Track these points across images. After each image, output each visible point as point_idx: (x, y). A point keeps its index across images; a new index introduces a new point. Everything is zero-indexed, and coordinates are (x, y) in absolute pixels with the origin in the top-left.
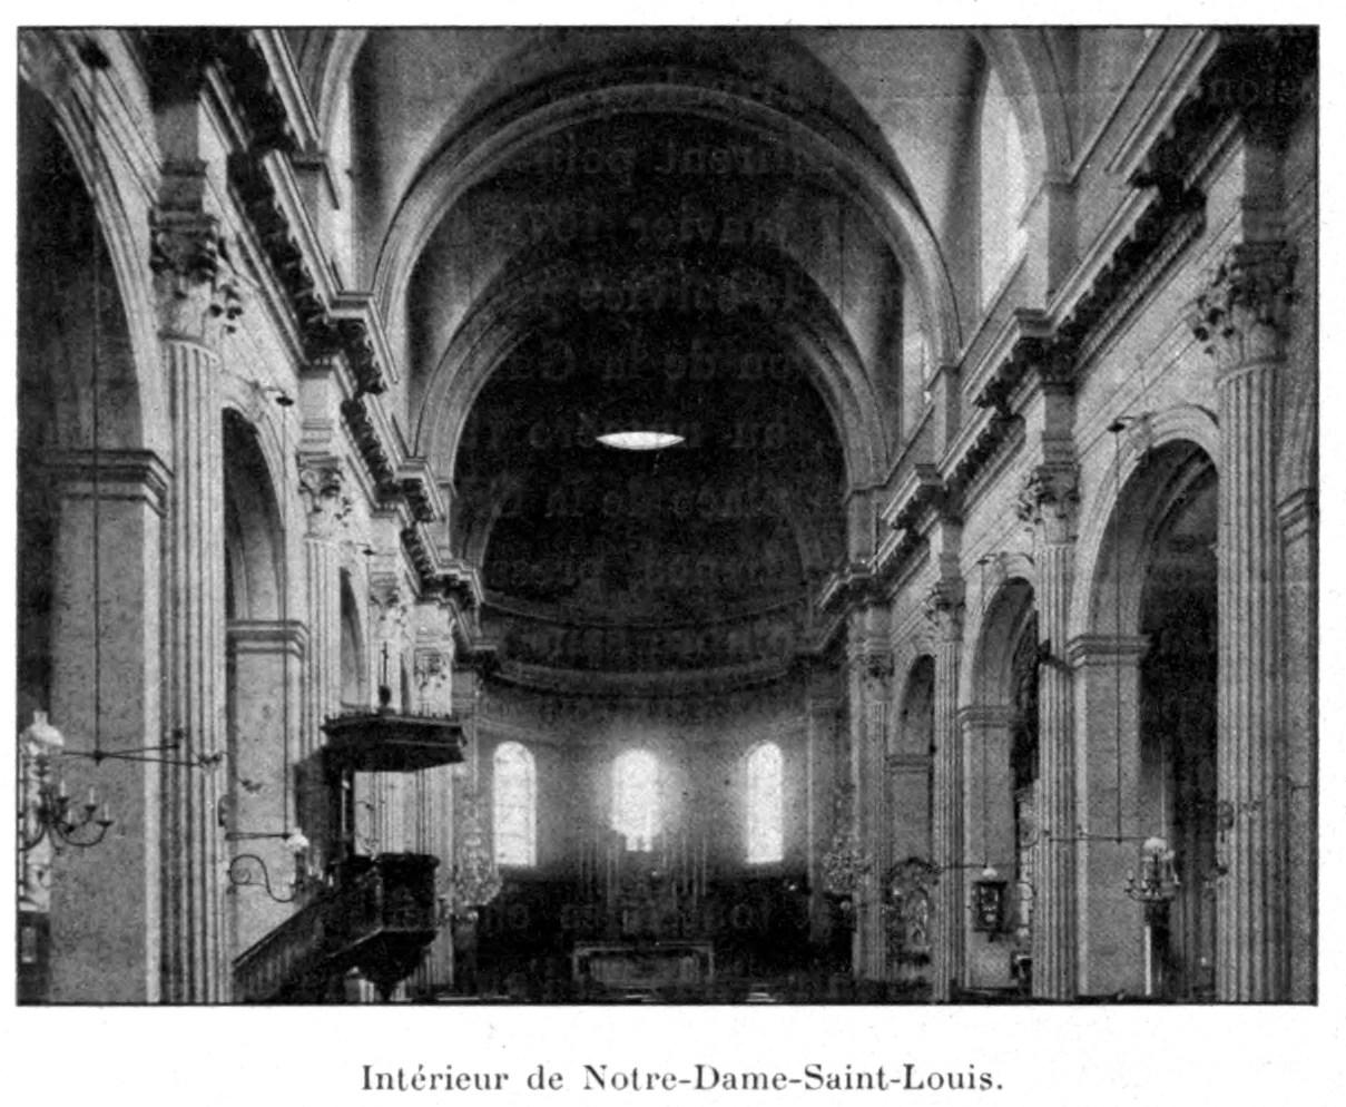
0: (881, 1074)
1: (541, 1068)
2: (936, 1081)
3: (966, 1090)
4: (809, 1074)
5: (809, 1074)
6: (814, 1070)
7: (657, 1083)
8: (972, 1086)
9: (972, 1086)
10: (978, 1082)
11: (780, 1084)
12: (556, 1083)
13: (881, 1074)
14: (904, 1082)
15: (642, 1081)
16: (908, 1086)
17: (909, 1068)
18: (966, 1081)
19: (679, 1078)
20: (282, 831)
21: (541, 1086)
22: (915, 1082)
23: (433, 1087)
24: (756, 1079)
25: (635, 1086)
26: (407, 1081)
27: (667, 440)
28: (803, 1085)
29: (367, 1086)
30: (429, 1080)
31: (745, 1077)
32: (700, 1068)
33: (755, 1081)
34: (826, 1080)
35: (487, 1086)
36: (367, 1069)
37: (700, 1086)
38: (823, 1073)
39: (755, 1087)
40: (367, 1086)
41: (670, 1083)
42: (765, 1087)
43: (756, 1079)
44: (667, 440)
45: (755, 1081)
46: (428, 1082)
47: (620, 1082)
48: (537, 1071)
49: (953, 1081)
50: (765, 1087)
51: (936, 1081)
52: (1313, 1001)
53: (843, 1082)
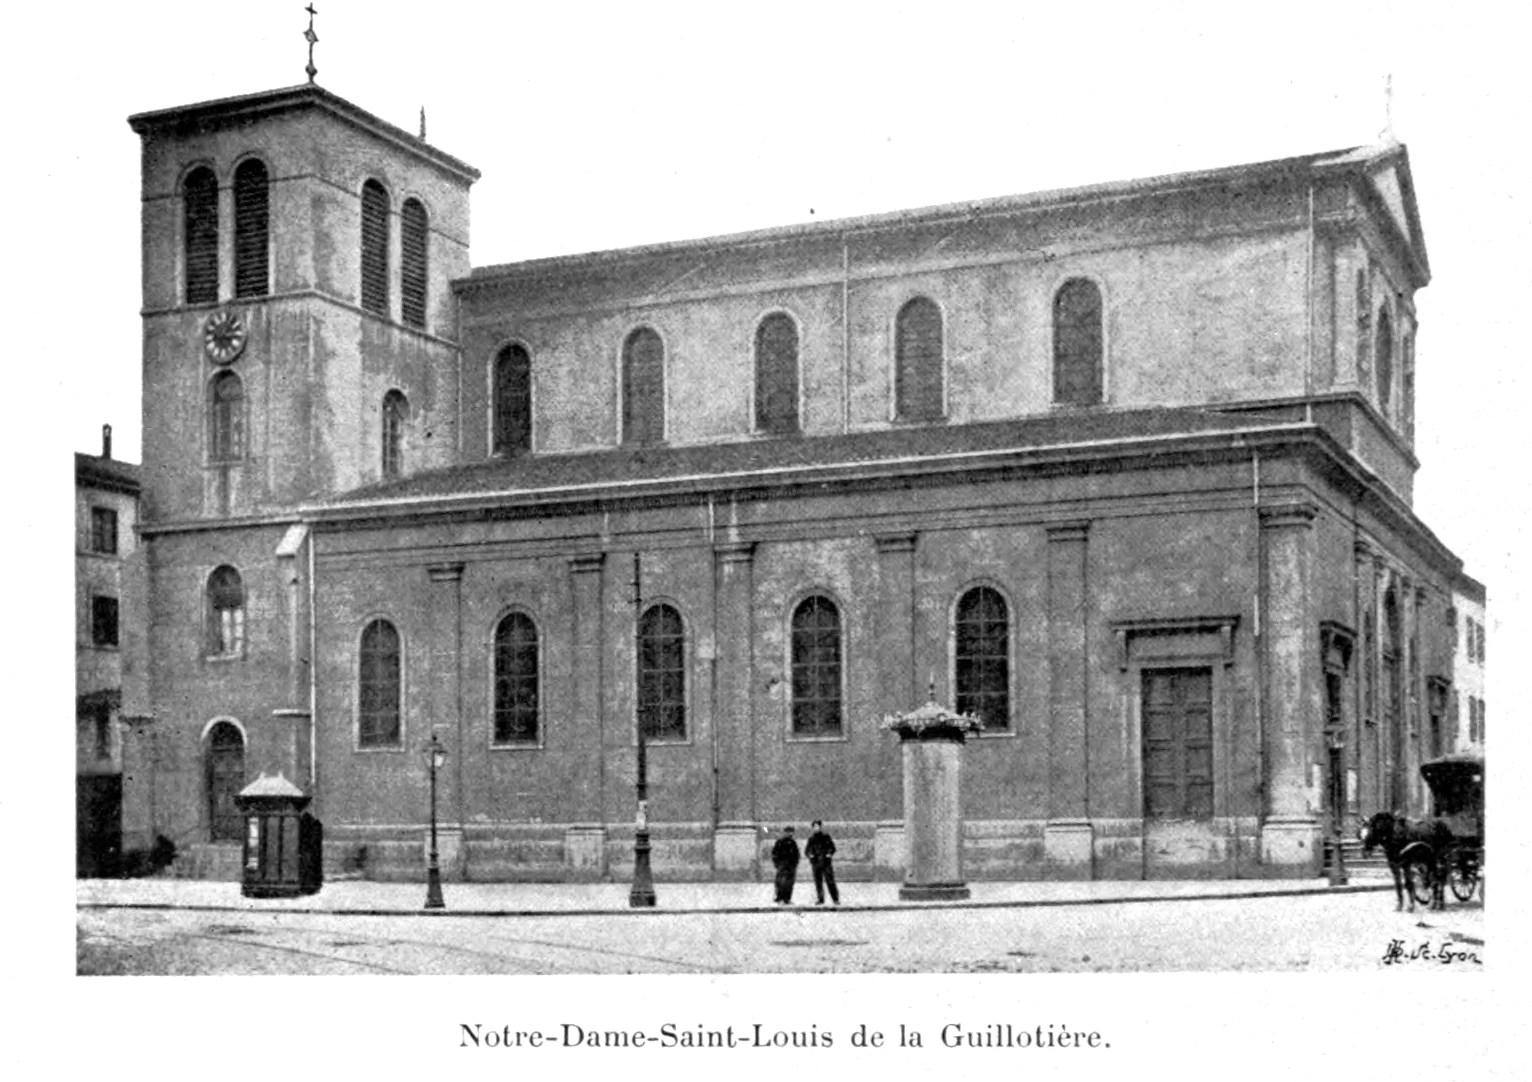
0: (730, 1033)
1: (863, 1027)
2: (781, 1039)
3: (696, 1049)
4: (664, 1033)
5: (664, 1033)
6: (669, 1029)
7: (525, 1041)
8: (814, 1044)
9: (814, 1044)
10: (819, 1040)
11: (638, 1041)
12: (877, 1041)
13: (730, 1033)
14: (563, 1040)
15: (512, 1037)
16: (757, 1044)
17: (757, 1027)
18: (984, 1040)
19: (647, 1036)
20: (1082, 804)
21: (863, 1044)
22: (762, 1041)
23: (1077, 1045)
24: (617, 1036)
25: (1039, 1044)
26: (1045, 1038)
27: (1403, 852)
28: (659, 1043)
29: (903, 1044)
30: (1073, 1037)
31: (607, 1035)
32: (566, 1027)
33: (615, 1039)
34: (680, 1038)
35: (804, 1044)
36: (903, 1027)
37: (566, 1044)
38: (678, 1033)
39: (617, 1044)
40: (903, 1044)
41: (536, 1041)
42: (626, 1044)
43: (617, 1036)
44: (1403, 852)
45: (615, 1039)
46: (1072, 1040)
47: (1024, 1040)
48: (860, 1030)
49: (798, 1040)
50: (626, 1044)
51: (781, 1039)
52: (80, 972)
53: (696, 1041)
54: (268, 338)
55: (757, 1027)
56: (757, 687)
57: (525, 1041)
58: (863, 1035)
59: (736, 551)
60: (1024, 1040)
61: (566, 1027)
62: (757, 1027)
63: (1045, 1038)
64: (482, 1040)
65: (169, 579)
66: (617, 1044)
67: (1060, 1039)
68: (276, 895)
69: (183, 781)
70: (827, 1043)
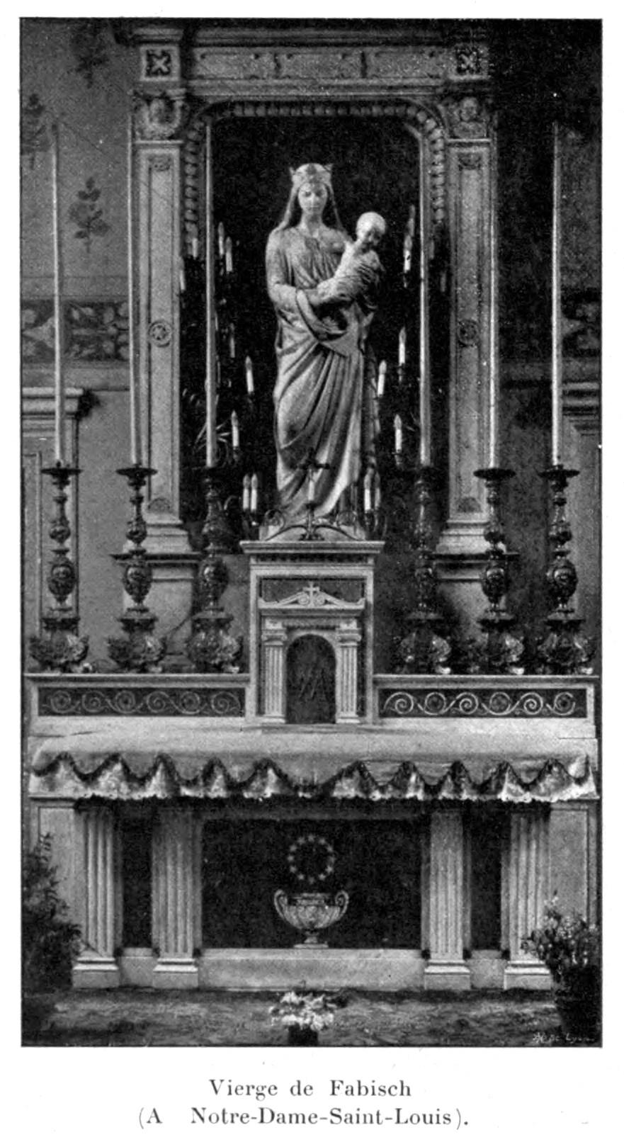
2: (415, 1119)
6: (335, 1112)
7: (237, 1119)
14: (259, 1119)
15: (228, 1117)
17: (398, 1110)
47: (214, 1118)
51: (415, 1119)
53: (355, 1119)
54: (172, 269)
57: (237, 1119)
59: (468, 526)
60: (214, 1118)
62: (398, 1110)
64: (206, 1119)
65: (175, 816)
68: (274, 579)
69: (71, 103)
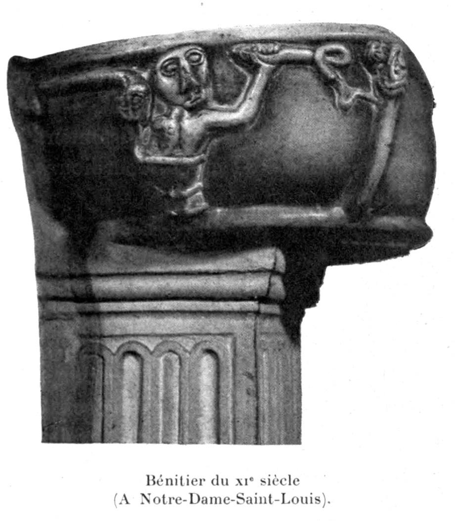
0: (270, 497)
2: (295, 500)
6: (240, 495)
7: (173, 501)
8: (311, 503)
10: (314, 501)
13: (270, 497)
15: (167, 500)
16: (283, 502)
22: (286, 501)
24: (216, 499)
26: (185, 481)
28: (235, 502)
31: (211, 498)
32: (191, 495)
34: (246, 500)
38: (245, 497)
39: (216, 503)
42: (220, 503)
43: (216, 499)
46: (199, 482)
48: (216, 478)
50: (220, 503)
51: (295, 500)
53: (254, 501)
55: (283, 494)
56: (125, 147)
57: (173, 501)
58: (217, 480)
61: (191, 495)
63: (185, 481)
64: (151, 501)
66: (216, 503)
67: (158, 482)
70: (318, 502)
